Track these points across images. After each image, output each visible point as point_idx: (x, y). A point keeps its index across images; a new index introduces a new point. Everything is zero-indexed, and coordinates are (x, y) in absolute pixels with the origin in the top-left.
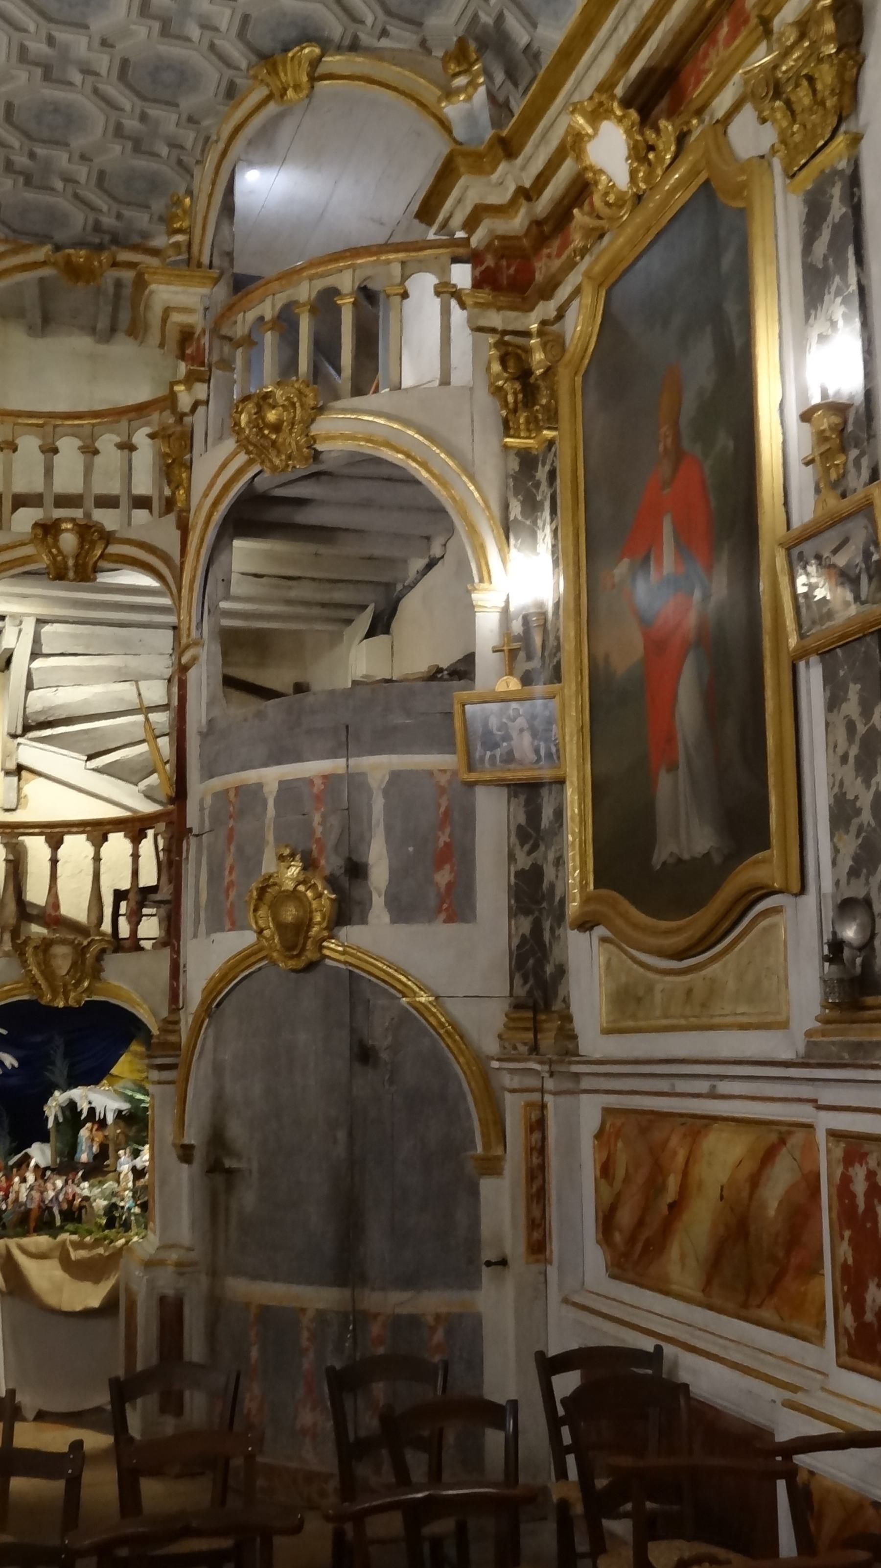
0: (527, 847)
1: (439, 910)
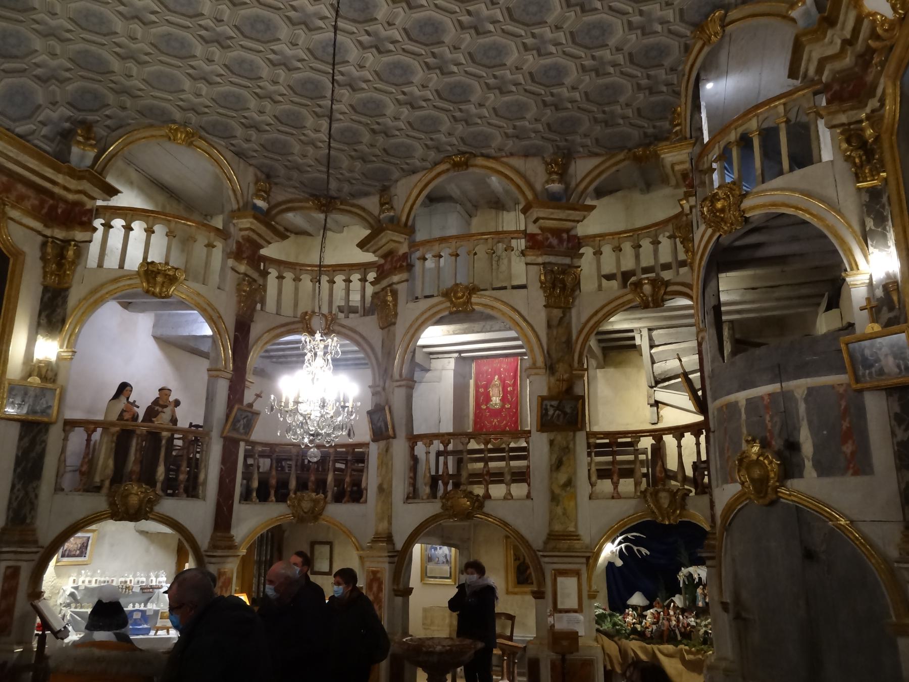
0: (903, 427)
1: (847, 468)
